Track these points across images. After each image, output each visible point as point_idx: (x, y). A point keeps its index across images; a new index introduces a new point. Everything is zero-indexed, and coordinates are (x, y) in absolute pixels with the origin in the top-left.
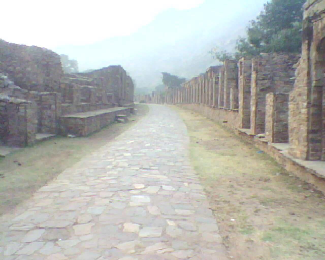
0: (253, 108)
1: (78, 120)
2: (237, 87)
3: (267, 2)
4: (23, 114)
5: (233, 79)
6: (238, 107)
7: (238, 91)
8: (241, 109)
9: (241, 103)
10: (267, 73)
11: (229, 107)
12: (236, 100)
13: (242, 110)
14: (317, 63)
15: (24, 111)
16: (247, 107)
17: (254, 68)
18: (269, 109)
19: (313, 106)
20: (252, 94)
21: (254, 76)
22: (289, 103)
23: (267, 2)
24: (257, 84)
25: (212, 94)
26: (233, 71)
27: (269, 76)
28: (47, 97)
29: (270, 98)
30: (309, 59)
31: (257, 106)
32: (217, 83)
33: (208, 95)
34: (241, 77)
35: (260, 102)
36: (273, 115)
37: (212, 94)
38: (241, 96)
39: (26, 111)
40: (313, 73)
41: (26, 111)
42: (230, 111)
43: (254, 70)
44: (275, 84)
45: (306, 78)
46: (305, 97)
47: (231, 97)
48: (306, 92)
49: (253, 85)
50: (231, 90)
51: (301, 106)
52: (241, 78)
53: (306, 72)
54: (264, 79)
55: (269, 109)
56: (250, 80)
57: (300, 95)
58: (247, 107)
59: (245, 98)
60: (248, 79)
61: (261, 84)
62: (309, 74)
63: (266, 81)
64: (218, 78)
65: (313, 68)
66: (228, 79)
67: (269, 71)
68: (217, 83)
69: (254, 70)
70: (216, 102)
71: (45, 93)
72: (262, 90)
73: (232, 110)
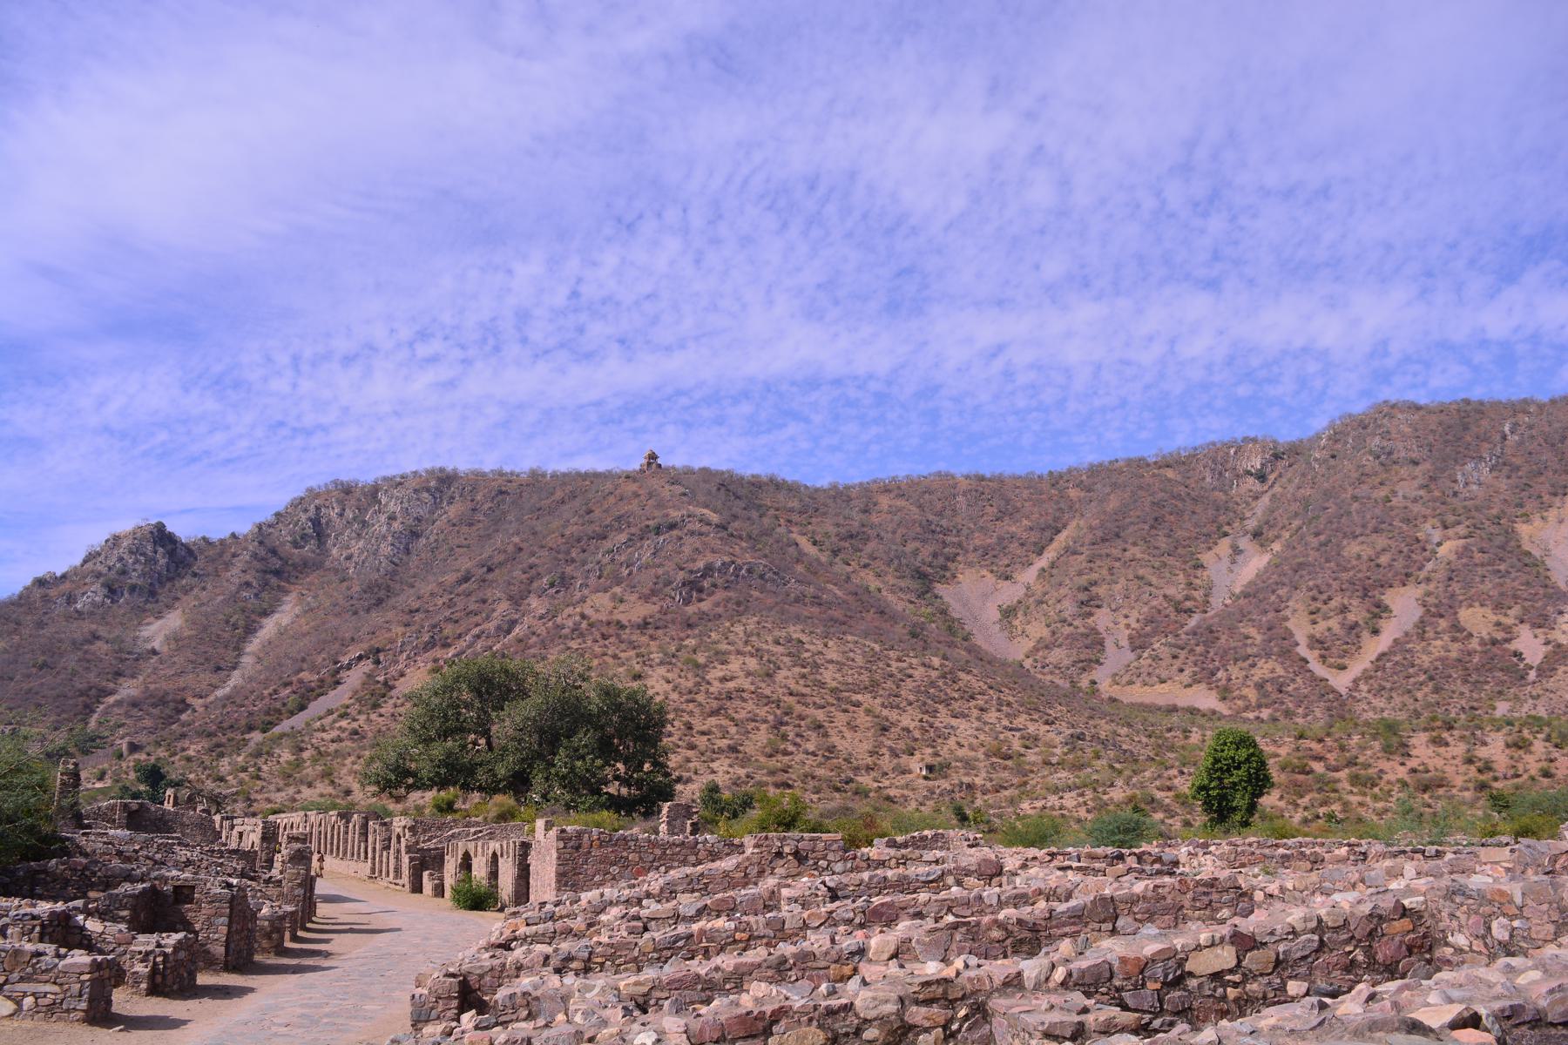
16: (374, 858)
29: (385, 853)
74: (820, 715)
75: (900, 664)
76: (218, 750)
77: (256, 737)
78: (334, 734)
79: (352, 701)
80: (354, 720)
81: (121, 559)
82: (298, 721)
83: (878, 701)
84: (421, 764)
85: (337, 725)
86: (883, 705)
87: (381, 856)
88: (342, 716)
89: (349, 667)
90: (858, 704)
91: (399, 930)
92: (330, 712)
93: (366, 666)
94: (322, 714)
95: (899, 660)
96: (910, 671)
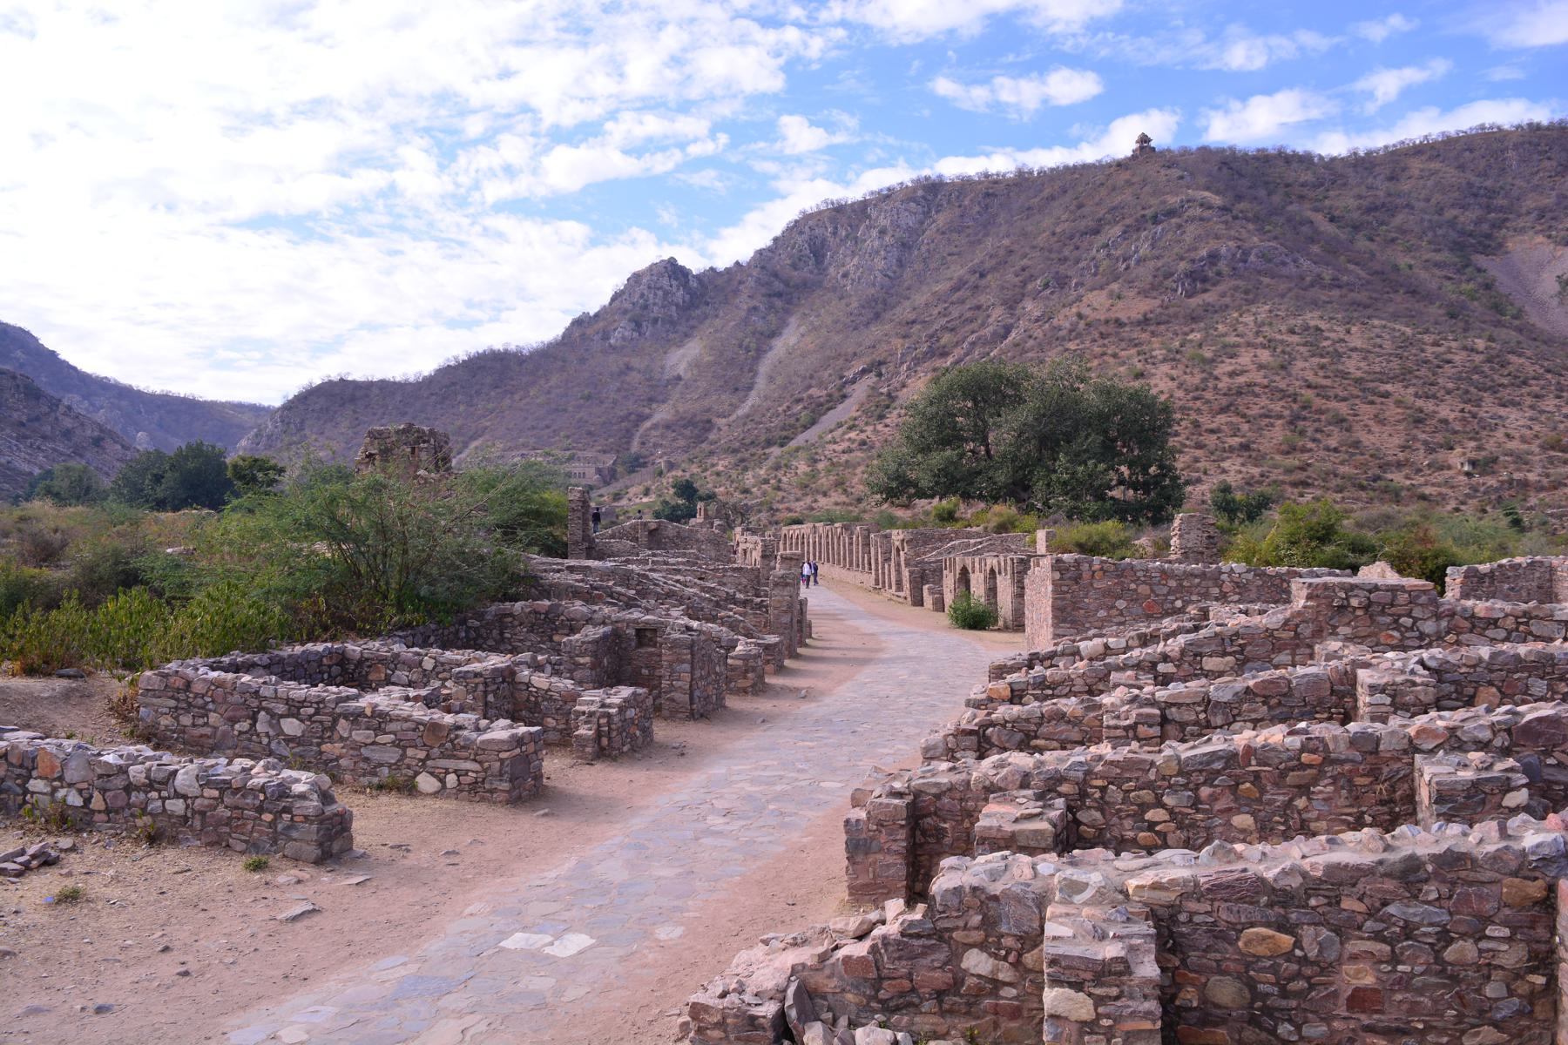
16: (877, 570)
74: (1343, 408)
75: (1436, 349)
78: (845, 445)
86: (1416, 395)
87: (883, 568)
89: (853, 381)
90: (1386, 395)
92: (840, 425)
94: (832, 427)
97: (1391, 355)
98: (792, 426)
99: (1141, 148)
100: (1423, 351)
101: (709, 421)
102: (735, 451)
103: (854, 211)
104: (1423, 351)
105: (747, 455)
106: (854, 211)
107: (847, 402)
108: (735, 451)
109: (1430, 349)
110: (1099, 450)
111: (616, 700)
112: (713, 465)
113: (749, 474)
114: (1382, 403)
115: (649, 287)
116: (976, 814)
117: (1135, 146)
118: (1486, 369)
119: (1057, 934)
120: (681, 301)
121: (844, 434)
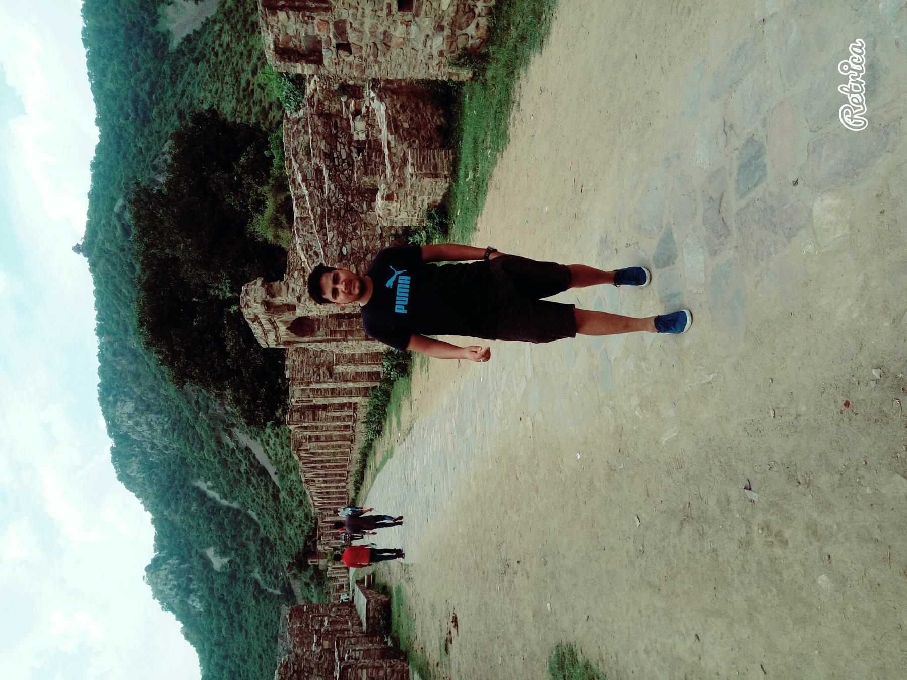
0: (351, 385)
1: (371, 607)
2: (325, 407)
3: (99, 385)
4: (362, 652)
5: (314, 414)
6: (351, 404)
7: (330, 405)
8: (354, 400)
9: (345, 400)
10: (312, 371)
11: (351, 416)
12: (342, 406)
13: (353, 399)
14: (312, 336)
15: (357, 653)
16: (349, 393)
17: (306, 386)
18: (351, 369)
19: (346, 336)
20: (335, 387)
21: (314, 386)
22: (360, 139)
23: (99, 385)
24: (325, 382)
25: (333, 447)
26: (304, 414)
27: (315, 369)
28: (341, 649)
29: (339, 369)
30: (308, 342)
31: (347, 381)
32: (318, 439)
33: (334, 454)
34: (314, 401)
35: (343, 378)
36: (355, 365)
37: (333, 447)
38: (336, 401)
39: (358, 650)
40: (320, 338)
41: (358, 650)
42: (355, 415)
43: (309, 386)
44: (324, 362)
45: (324, 343)
46: (339, 343)
47: (338, 414)
48: (335, 343)
49: (325, 386)
50: (329, 414)
51: (347, 346)
52: (320, 401)
53: (319, 344)
54: (319, 375)
55: (351, 369)
56: (318, 390)
57: (337, 346)
58: (349, 393)
59: (339, 395)
60: (317, 393)
61: (324, 377)
62: (320, 341)
63: (321, 372)
64: (310, 437)
65: (315, 339)
66: (314, 420)
67: (310, 370)
68: (318, 439)
69: (309, 386)
70: (344, 438)
71: (336, 654)
72: (331, 376)
73: (354, 412)
74: (256, 109)
75: (220, 54)
76: (290, 517)
77: (283, 494)
78: (279, 448)
79: (258, 439)
80: (269, 436)
81: (171, 589)
82: (271, 470)
83: (246, 67)
84: (543, 31)
85: (272, 446)
86: (248, 63)
87: (343, 378)
88: (268, 445)
89: (237, 442)
90: (248, 82)
91: (762, 666)
92: (266, 451)
93: (236, 431)
94: (266, 457)
95: (216, 55)
96: (225, 46)
97: (222, 84)
98: (266, 485)
99: (82, 251)
100: (220, 62)
101: (262, 540)
102: (281, 523)
103: (121, 443)
104: (220, 62)
105: (284, 515)
106: (121, 443)
107: (250, 446)
108: (281, 523)
109: (220, 58)
110: (197, 112)
111: (178, 90)
112: (290, 538)
113: (296, 513)
114: (253, 84)
115: (166, 585)
116: (299, 569)
117: (81, 255)
118: (233, 21)
119: (626, 288)
120: (177, 561)
121: (271, 448)
